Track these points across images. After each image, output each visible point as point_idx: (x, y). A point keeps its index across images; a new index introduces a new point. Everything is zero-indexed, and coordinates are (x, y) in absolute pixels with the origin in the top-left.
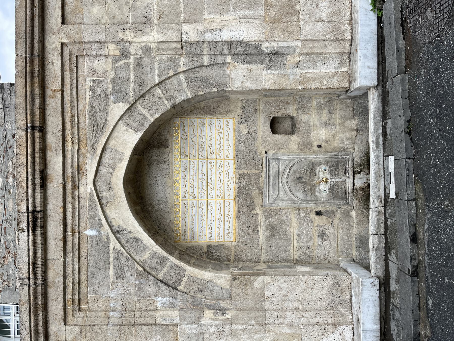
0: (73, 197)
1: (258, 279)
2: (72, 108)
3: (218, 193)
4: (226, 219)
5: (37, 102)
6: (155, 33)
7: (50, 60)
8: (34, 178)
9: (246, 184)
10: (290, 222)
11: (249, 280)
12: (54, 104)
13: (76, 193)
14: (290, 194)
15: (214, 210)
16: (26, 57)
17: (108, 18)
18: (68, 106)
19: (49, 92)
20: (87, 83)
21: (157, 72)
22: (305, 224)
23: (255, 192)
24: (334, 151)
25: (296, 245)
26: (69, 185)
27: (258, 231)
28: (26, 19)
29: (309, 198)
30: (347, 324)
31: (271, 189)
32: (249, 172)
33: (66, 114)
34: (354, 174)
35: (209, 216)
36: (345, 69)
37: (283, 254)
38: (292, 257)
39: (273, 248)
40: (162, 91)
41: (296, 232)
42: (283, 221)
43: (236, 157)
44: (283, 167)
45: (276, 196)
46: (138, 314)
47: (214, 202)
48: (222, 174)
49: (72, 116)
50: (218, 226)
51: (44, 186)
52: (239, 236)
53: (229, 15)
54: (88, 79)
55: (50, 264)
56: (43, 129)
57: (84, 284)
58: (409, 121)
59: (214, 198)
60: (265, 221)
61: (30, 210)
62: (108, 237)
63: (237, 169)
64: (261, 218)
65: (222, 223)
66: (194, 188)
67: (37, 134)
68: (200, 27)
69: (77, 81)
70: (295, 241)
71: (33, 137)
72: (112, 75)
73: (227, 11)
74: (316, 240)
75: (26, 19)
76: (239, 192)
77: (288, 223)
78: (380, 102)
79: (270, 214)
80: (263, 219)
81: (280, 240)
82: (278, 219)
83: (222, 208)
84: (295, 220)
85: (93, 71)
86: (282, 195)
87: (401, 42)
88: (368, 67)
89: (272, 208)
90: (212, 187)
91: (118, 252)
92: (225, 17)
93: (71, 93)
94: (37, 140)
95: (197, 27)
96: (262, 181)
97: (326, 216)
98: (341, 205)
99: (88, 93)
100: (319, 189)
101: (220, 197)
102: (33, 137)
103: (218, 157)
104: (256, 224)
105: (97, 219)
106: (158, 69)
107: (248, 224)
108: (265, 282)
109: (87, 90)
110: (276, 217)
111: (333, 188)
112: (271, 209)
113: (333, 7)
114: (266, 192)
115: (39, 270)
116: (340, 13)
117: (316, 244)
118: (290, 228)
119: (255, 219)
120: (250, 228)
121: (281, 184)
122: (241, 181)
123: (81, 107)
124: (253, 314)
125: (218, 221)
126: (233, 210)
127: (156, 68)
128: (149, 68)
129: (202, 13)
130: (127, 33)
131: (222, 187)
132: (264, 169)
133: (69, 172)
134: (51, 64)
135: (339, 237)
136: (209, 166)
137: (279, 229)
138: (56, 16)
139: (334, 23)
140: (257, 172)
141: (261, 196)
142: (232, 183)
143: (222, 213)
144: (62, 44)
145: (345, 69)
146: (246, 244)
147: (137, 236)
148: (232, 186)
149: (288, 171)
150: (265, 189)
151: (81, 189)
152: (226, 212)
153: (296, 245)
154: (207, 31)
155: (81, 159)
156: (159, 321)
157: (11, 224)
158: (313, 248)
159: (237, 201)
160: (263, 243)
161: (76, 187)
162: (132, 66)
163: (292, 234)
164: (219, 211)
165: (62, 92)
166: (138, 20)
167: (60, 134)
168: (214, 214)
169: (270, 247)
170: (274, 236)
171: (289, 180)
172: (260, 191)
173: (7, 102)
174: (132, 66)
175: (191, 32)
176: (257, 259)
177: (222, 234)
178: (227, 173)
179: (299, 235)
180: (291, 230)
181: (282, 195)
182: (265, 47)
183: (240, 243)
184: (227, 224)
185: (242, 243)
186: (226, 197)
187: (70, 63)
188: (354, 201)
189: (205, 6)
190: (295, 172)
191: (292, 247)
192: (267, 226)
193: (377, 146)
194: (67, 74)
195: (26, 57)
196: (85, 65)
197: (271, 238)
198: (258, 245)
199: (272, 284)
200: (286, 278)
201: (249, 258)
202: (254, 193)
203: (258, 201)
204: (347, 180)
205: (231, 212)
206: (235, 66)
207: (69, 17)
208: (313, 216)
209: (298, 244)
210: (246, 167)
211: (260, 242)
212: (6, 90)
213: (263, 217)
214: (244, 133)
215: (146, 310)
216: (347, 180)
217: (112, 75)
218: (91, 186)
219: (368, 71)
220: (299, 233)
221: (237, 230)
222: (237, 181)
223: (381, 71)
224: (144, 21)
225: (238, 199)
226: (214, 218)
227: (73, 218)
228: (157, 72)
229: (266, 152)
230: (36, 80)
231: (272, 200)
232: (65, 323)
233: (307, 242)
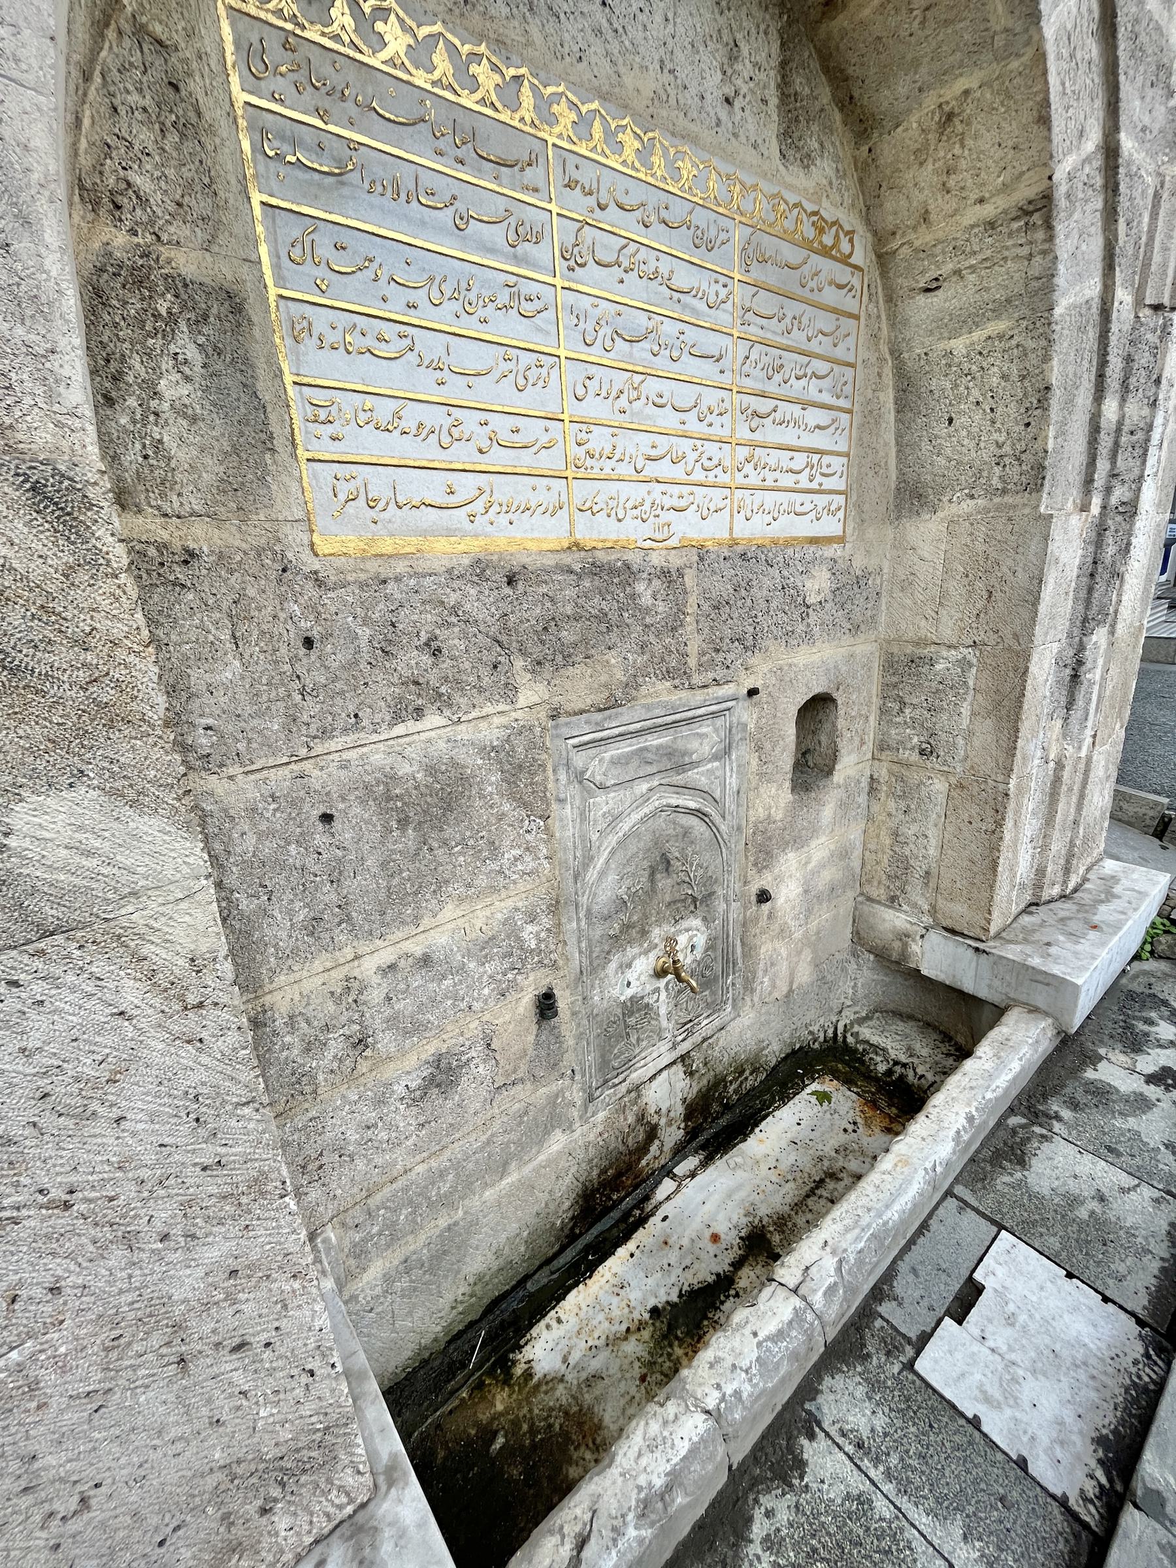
1: (149, 826)
3: (599, 440)
4: (467, 485)
9: (648, 611)
10: (494, 890)
11: (113, 718)
15: (505, 395)
22: (489, 968)
23: (616, 663)
25: (368, 967)
27: (419, 713)
31: (625, 748)
35: (471, 357)
37: (291, 913)
38: (282, 979)
39: (320, 839)
42: (494, 849)
43: (739, 549)
44: (703, 782)
45: (598, 779)
48: (678, 473)
50: (412, 415)
52: (363, 585)
59: (571, 409)
60: (485, 750)
63: (701, 559)
64: (497, 720)
65: (428, 452)
66: (617, 272)
70: (386, 956)
74: (411, 1061)
76: (612, 571)
77: (482, 881)
79: (520, 768)
80: (491, 733)
81: (384, 865)
82: (501, 817)
83: (525, 459)
84: (501, 907)
86: (603, 803)
89: (550, 772)
90: (623, 402)
96: (660, 693)
97: (537, 1043)
98: (583, 1075)
100: (634, 958)
101: (581, 452)
104: (458, 698)
107: (452, 641)
108: (133, 915)
110: (506, 807)
111: (639, 1010)
112: (543, 766)
114: (616, 723)
117: (389, 1072)
118: (461, 900)
119: (486, 681)
120: (427, 660)
121: (644, 787)
122: (656, 583)
125: (436, 417)
126: (516, 533)
131: (625, 470)
132: (699, 696)
135: (447, 1154)
136: (711, 398)
137: (445, 843)
140: (692, 662)
141: (600, 698)
142: (647, 530)
143: (499, 458)
146: (308, 643)
148: (633, 531)
149: (692, 805)
150: (626, 719)
152: (505, 488)
153: (368, 967)
158: (363, 1067)
159: (567, 559)
160: (345, 765)
163: (426, 922)
164: (505, 436)
168: (485, 392)
169: (327, 818)
170: (403, 823)
171: (660, 821)
172: (619, 694)
176: (204, 741)
177: (370, 444)
178: (682, 503)
179: (426, 961)
180: (450, 906)
182: (1100, 636)
183: (311, 590)
184: (431, 487)
185: (314, 610)
186: (581, 491)
188: (601, 1115)
190: (685, 834)
191: (348, 952)
192: (455, 764)
197: (383, 811)
198: (325, 733)
199: (132, 994)
200: (239, 1093)
201: (197, 677)
202: (613, 658)
203: (579, 686)
204: (664, 1047)
205: (503, 519)
208: (530, 988)
209: (376, 979)
210: (706, 607)
211: (350, 739)
213: (503, 733)
214: (808, 584)
216: (664, 1047)
220: (438, 956)
221: (401, 567)
222: (656, 559)
225: (577, 567)
226: (455, 390)
229: (753, 692)
231: (579, 760)
233: (392, 1022)
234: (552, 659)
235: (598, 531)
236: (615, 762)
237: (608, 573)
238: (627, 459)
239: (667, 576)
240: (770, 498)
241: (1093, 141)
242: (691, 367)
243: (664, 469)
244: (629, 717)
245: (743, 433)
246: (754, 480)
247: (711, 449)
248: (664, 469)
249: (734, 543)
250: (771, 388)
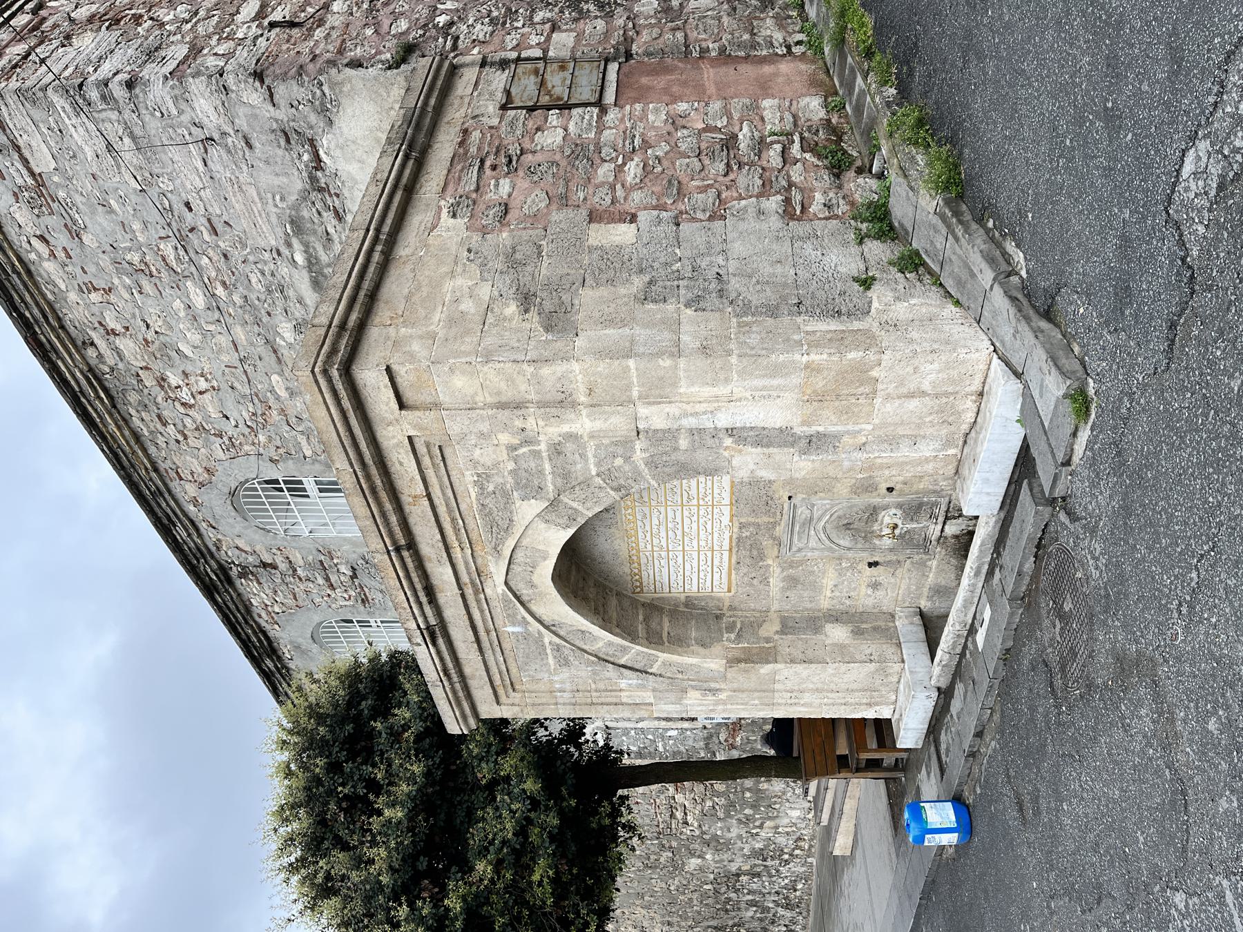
0: (478, 601)
2: (450, 511)
5: (393, 519)
6: (586, 420)
7: (394, 459)
8: (417, 597)
12: (419, 516)
13: (482, 596)
14: (827, 542)
16: (355, 471)
17: (487, 395)
18: (442, 510)
19: (405, 499)
20: (466, 481)
21: (592, 460)
23: (766, 543)
24: (916, 493)
25: (828, 594)
26: (469, 591)
28: (333, 421)
29: (860, 546)
30: (887, 704)
31: (796, 537)
32: (759, 520)
33: (442, 519)
34: (947, 518)
36: (952, 451)
40: (604, 480)
41: (831, 583)
46: (594, 694)
47: (695, 555)
48: (709, 523)
49: (453, 520)
51: (433, 600)
53: (729, 387)
54: (468, 473)
55: (463, 662)
56: (412, 545)
57: (514, 671)
58: (1008, 650)
61: (422, 626)
62: (539, 633)
67: (405, 554)
68: (673, 409)
69: (449, 476)
71: (402, 559)
72: (511, 466)
73: (727, 380)
75: (333, 421)
78: (997, 529)
80: (778, 570)
85: (475, 463)
87: (1029, 565)
88: (988, 494)
91: (558, 645)
92: (723, 390)
93: (444, 494)
94: (409, 561)
95: (667, 410)
99: (471, 490)
102: (402, 559)
103: (701, 502)
105: (519, 617)
106: (595, 456)
109: (470, 487)
113: (951, 372)
115: (452, 671)
116: (962, 380)
123: (463, 507)
124: (757, 694)
127: (590, 455)
128: (577, 456)
129: (675, 384)
130: (531, 420)
132: (785, 517)
133: (465, 578)
134: (397, 465)
138: (384, 399)
139: (944, 400)
144: (409, 438)
145: (952, 451)
147: (583, 628)
148: (727, 535)
151: (488, 591)
154: (686, 415)
155: (479, 561)
156: (624, 700)
157: (255, 366)
161: (479, 590)
162: (545, 454)
165: (429, 496)
166: (548, 397)
167: (441, 545)
173: (138, 131)
174: (545, 454)
175: (655, 417)
181: (813, 543)
187: (431, 458)
189: (682, 374)
193: (977, 574)
194: (430, 473)
195: (355, 471)
196: (458, 458)
206: (740, 451)
207: (409, 395)
212: (121, 102)
215: (606, 690)
217: (511, 466)
218: (501, 588)
219: (986, 498)
223: (1011, 492)
224: (559, 399)
227: (484, 620)
228: (592, 460)
229: (790, 498)
230: (383, 495)
231: (794, 549)
232: (498, 703)
234: (762, 557)
235: (726, 546)
236: (799, 540)
237: (739, 543)
238: (118, 91)
239: (742, 526)
240: (716, 491)
241: (745, 686)
242: (679, 519)
243: (709, 527)
244: (785, 539)
245: (695, 502)
246: (710, 497)
247: (701, 513)
248: (709, 527)
249: (731, 504)
250: (679, 492)
